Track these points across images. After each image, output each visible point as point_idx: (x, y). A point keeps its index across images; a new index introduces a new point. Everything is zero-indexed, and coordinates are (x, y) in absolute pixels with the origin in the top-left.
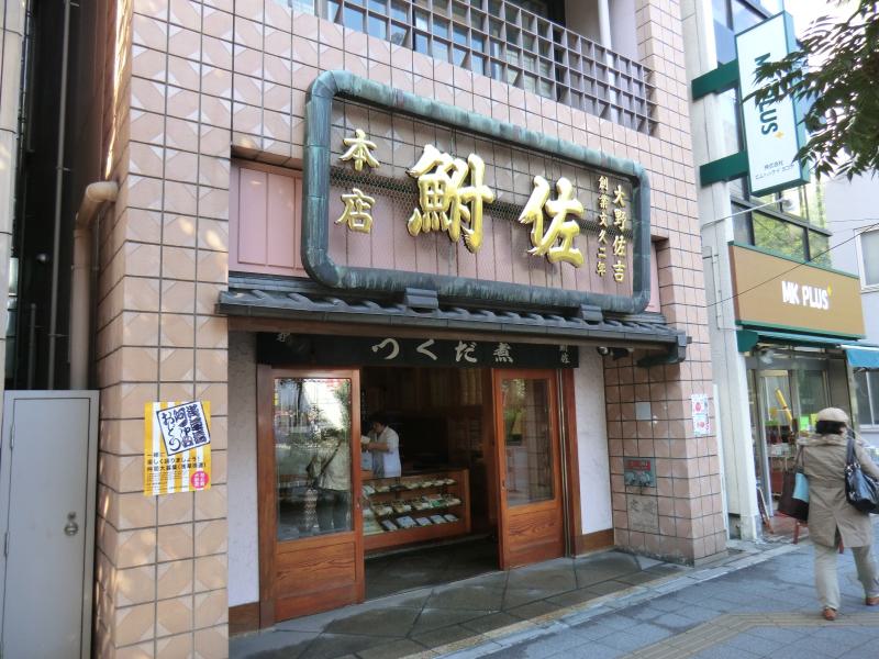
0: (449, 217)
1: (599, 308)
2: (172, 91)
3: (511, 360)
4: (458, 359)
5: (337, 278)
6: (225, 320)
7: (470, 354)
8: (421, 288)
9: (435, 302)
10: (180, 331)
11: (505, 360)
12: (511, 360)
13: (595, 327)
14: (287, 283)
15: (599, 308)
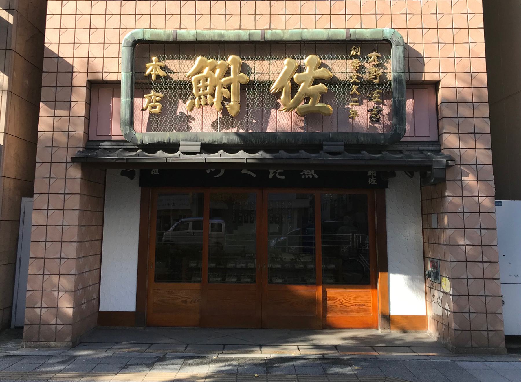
0: (229, 68)
1: (343, 143)
2: (457, 88)
3: (316, 176)
4: (271, 176)
5: (137, 140)
6: (80, 167)
7: (280, 174)
8: (190, 140)
9: (343, 148)
10: (59, 170)
11: (311, 176)
12: (316, 176)
13: (338, 157)
14: (92, 147)
15: (343, 143)
